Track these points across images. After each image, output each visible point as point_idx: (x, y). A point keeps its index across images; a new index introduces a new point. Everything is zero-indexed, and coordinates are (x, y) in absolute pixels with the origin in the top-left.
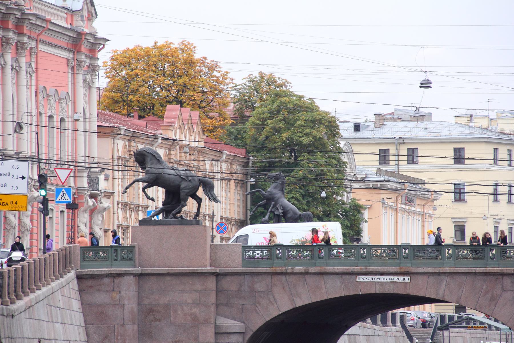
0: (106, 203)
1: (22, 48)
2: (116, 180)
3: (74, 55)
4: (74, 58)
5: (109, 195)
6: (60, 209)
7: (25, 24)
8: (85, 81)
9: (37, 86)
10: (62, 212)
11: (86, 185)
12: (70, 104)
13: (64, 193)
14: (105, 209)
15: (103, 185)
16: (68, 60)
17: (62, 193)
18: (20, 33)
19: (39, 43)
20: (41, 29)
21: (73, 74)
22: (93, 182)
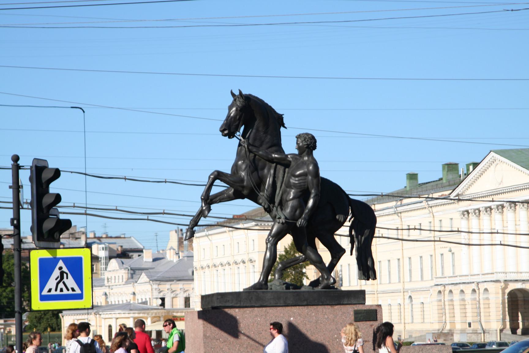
13: (62, 273)
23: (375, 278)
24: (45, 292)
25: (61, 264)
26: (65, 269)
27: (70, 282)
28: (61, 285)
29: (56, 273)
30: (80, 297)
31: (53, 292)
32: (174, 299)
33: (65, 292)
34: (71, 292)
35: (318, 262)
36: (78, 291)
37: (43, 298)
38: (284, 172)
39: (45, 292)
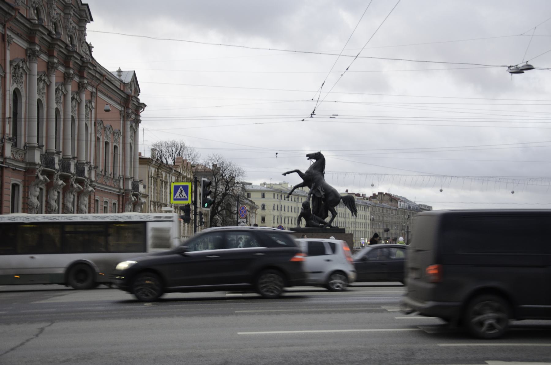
0: (143, 200)
1: (83, 87)
2: (150, 189)
3: (124, 108)
4: (124, 111)
5: (146, 196)
6: (113, 202)
7: (36, 36)
8: (131, 126)
9: (96, 118)
10: (114, 204)
11: (130, 188)
12: (121, 138)
13: (181, 191)
14: (142, 203)
15: (141, 189)
16: (121, 111)
17: (179, 191)
18: (82, 77)
19: (7, 29)
20: (99, 82)
21: (124, 120)
22: (135, 187)
24: (175, 198)
25: (181, 187)
27: (184, 194)
29: (179, 191)
30: (187, 199)
32: (296, 174)
37: (175, 200)
39: (175, 198)
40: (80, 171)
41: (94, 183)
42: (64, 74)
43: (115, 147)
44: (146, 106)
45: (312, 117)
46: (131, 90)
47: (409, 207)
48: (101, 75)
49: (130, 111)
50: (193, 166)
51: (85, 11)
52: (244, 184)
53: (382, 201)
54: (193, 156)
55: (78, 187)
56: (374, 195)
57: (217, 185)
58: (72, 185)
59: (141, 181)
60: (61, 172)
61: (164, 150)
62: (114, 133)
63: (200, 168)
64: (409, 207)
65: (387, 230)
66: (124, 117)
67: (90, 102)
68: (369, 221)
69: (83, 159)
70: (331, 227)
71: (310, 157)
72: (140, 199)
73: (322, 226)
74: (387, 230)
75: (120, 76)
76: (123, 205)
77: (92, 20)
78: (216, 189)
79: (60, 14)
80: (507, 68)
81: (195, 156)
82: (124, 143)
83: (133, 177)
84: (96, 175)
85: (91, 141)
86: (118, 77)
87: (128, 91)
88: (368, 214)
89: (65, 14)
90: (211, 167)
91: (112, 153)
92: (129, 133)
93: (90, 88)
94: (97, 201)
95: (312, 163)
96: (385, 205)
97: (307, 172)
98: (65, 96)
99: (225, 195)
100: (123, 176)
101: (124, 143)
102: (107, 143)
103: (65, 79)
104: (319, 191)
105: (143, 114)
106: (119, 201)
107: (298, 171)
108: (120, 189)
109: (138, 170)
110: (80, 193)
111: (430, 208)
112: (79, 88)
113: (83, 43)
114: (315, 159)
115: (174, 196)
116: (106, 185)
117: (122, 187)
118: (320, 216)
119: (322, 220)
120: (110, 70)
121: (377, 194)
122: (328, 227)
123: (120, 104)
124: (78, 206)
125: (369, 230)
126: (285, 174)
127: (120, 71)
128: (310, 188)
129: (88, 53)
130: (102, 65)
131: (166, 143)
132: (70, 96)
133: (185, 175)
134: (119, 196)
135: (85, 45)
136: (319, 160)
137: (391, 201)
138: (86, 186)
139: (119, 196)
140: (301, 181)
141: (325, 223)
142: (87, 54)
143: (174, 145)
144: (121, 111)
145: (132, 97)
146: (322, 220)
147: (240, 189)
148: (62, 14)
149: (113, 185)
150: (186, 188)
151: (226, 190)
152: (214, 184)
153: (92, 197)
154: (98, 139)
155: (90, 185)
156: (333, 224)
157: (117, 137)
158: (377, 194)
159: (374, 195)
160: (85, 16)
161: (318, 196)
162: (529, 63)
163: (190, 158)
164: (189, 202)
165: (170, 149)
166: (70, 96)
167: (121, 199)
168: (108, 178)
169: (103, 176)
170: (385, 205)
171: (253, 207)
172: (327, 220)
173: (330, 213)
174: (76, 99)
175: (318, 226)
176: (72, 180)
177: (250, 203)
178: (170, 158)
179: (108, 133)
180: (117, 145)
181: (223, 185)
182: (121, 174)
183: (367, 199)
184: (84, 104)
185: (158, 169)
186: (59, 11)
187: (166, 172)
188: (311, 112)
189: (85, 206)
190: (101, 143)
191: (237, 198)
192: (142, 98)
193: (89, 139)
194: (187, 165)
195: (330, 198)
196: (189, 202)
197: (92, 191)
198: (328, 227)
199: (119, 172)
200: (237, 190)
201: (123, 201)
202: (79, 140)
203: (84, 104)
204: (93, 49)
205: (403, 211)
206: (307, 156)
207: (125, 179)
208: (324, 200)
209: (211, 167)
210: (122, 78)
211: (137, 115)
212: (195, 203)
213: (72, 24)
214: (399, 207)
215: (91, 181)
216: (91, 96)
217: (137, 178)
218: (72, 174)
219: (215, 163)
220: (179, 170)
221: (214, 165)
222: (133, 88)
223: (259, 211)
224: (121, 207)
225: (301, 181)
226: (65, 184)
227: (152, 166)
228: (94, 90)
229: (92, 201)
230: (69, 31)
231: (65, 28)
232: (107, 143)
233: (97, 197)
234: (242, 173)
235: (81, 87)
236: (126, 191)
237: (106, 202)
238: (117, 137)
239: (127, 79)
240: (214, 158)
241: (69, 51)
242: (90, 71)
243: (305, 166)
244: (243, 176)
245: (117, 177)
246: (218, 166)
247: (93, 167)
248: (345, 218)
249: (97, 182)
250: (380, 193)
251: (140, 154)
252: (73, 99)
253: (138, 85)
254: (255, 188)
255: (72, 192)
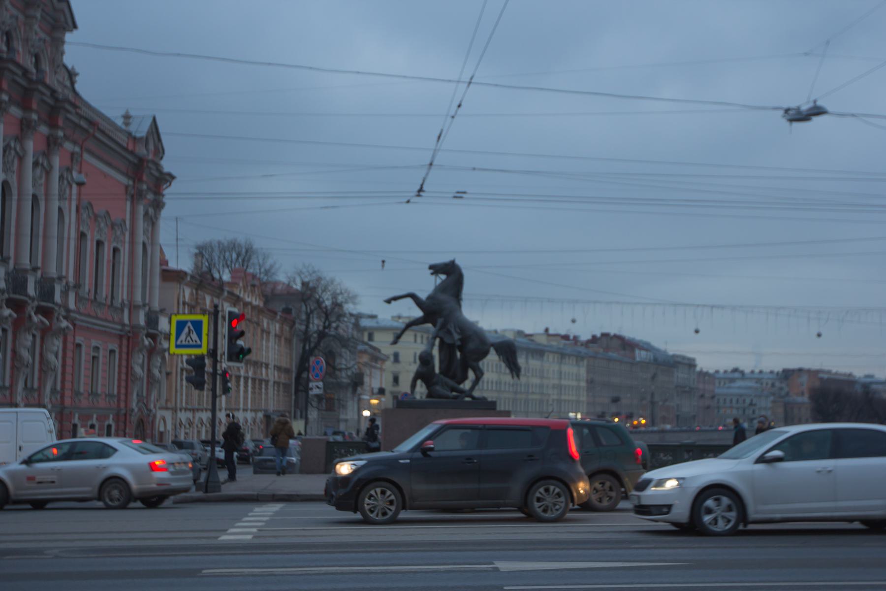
3: (134, 182)
4: (134, 187)
8: (146, 214)
9: (79, 200)
10: (112, 352)
13: (190, 330)
16: (127, 187)
22: (152, 321)
23: (173, 177)
24: (179, 343)
25: (189, 324)
26: (192, 328)
27: (194, 336)
28: (189, 338)
29: (186, 330)
30: (200, 346)
31: (184, 343)
32: (409, 301)
33: (191, 342)
34: (194, 343)
35: (364, 352)
36: (199, 342)
37: (177, 346)
38: (381, 376)
39: (179, 343)
40: (46, 292)
41: (72, 315)
42: (21, 121)
43: (116, 250)
44: (173, 177)
45: (419, 196)
46: (147, 150)
47: (655, 360)
48: (92, 123)
49: (145, 187)
50: (265, 284)
51: (63, 11)
52: (359, 317)
53: (607, 349)
54: (267, 266)
55: (42, 322)
56: (594, 337)
57: (308, 316)
58: (30, 317)
59: (162, 311)
60: (8, 293)
61: (216, 255)
62: (113, 226)
63: (279, 287)
64: (655, 360)
65: (616, 400)
66: (132, 196)
67: (69, 170)
68: (583, 384)
69: (53, 271)
70: (473, 398)
71: (436, 269)
72: (160, 343)
73: (455, 398)
74: (616, 400)
75: (127, 124)
76: (128, 354)
77: (75, 26)
78: (307, 327)
79: (17, 18)
80: (782, 112)
81: (272, 266)
82: (132, 243)
83: (148, 304)
84: (79, 299)
85: (69, 239)
86: (124, 127)
87: (141, 151)
88: (583, 371)
89: (27, 17)
90: (298, 286)
91: (108, 261)
92: (141, 224)
93: (68, 146)
94: (79, 346)
95: (439, 281)
96: (613, 354)
97: (430, 298)
98: (21, 159)
99: (322, 335)
100: (130, 302)
101: (132, 243)
102: (99, 244)
103: (22, 130)
104: (449, 332)
105: (169, 192)
106: (120, 346)
107: (413, 296)
108: (124, 325)
109: (157, 292)
110: (45, 332)
111: (691, 364)
112: (49, 145)
113: (58, 66)
114: (443, 273)
115: (177, 338)
116: (97, 318)
117: (126, 321)
118: (453, 378)
119: (456, 385)
120: (108, 113)
121: (599, 335)
122: (467, 399)
123: (126, 175)
124: (41, 355)
125: (584, 398)
126: (389, 301)
127: (127, 117)
128: (434, 325)
129: (68, 83)
130: (93, 104)
131: (219, 243)
132: (29, 160)
133: (248, 299)
134: (121, 337)
135: (63, 70)
136: (451, 275)
137: (624, 349)
138: (58, 319)
139: (121, 337)
140: (418, 313)
141: (462, 392)
142: (65, 86)
143: (233, 246)
144: (127, 187)
145: (148, 161)
146: (456, 385)
147: (351, 326)
148: (21, 17)
149: (110, 318)
150: (198, 325)
151: (325, 327)
152: (304, 317)
153: (70, 338)
154: (82, 236)
155: (65, 318)
156: (476, 394)
157: (118, 233)
158: (599, 335)
159: (594, 337)
160: (63, 19)
161: (448, 340)
162: (819, 103)
163: (262, 270)
164: (204, 350)
165: (227, 254)
166: (29, 160)
167: (125, 342)
168: (100, 305)
169: (92, 302)
170: (613, 354)
171: (376, 357)
172: (467, 385)
173: (471, 375)
174: (42, 165)
175: (447, 397)
176: (29, 308)
177: (370, 350)
178: (227, 271)
179: (102, 225)
180: (119, 246)
181: (319, 318)
182: (125, 297)
183: (582, 345)
184: (56, 175)
185: (197, 290)
186: (15, 12)
187: (212, 295)
188: (418, 187)
189: (57, 357)
190: (89, 243)
191: (344, 342)
192: (167, 165)
193: (66, 235)
194: (256, 284)
195: (471, 346)
196: (204, 350)
197: (67, 327)
198: (467, 399)
199: (122, 294)
200: (345, 329)
201: (128, 347)
202: (45, 237)
203: (56, 175)
204: (78, 79)
205: (644, 364)
206: (431, 267)
207: (133, 308)
208: (461, 348)
209: (298, 286)
210: (132, 128)
211: (158, 192)
212: (213, 353)
213: (38, 33)
214: (638, 359)
215: (68, 311)
216: (72, 160)
217: (156, 306)
218: (29, 297)
219: (306, 280)
220: (237, 292)
221: (304, 284)
222: (151, 147)
223: (389, 365)
224: (124, 356)
225: (418, 313)
226: (15, 315)
227: (187, 285)
228: (77, 149)
229: (70, 346)
230: (33, 46)
231: (26, 41)
232: (99, 244)
233: (79, 340)
234: (353, 298)
235: (52, 143)
236: (135, 328)
237: (97, 349)
238: (118, 233)
239: (141, 129)
240: (304, 270)
241: (30, 81)
242: (69, 116)
243: (427, 285)
244: (354, 303)
245: (117, 303)
246: (311, 285)
247: (71, 285)
248: (542, 377)
249: (79, 313)
250: (605, 335)
251: (164, 262)
252: (36, 164)
253: (160, 140)
254: (382, 324)
255: (29, 330)
